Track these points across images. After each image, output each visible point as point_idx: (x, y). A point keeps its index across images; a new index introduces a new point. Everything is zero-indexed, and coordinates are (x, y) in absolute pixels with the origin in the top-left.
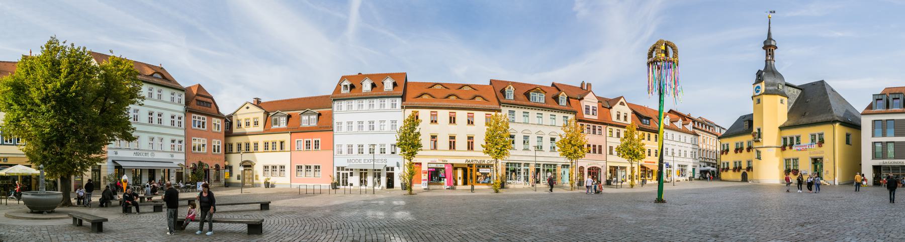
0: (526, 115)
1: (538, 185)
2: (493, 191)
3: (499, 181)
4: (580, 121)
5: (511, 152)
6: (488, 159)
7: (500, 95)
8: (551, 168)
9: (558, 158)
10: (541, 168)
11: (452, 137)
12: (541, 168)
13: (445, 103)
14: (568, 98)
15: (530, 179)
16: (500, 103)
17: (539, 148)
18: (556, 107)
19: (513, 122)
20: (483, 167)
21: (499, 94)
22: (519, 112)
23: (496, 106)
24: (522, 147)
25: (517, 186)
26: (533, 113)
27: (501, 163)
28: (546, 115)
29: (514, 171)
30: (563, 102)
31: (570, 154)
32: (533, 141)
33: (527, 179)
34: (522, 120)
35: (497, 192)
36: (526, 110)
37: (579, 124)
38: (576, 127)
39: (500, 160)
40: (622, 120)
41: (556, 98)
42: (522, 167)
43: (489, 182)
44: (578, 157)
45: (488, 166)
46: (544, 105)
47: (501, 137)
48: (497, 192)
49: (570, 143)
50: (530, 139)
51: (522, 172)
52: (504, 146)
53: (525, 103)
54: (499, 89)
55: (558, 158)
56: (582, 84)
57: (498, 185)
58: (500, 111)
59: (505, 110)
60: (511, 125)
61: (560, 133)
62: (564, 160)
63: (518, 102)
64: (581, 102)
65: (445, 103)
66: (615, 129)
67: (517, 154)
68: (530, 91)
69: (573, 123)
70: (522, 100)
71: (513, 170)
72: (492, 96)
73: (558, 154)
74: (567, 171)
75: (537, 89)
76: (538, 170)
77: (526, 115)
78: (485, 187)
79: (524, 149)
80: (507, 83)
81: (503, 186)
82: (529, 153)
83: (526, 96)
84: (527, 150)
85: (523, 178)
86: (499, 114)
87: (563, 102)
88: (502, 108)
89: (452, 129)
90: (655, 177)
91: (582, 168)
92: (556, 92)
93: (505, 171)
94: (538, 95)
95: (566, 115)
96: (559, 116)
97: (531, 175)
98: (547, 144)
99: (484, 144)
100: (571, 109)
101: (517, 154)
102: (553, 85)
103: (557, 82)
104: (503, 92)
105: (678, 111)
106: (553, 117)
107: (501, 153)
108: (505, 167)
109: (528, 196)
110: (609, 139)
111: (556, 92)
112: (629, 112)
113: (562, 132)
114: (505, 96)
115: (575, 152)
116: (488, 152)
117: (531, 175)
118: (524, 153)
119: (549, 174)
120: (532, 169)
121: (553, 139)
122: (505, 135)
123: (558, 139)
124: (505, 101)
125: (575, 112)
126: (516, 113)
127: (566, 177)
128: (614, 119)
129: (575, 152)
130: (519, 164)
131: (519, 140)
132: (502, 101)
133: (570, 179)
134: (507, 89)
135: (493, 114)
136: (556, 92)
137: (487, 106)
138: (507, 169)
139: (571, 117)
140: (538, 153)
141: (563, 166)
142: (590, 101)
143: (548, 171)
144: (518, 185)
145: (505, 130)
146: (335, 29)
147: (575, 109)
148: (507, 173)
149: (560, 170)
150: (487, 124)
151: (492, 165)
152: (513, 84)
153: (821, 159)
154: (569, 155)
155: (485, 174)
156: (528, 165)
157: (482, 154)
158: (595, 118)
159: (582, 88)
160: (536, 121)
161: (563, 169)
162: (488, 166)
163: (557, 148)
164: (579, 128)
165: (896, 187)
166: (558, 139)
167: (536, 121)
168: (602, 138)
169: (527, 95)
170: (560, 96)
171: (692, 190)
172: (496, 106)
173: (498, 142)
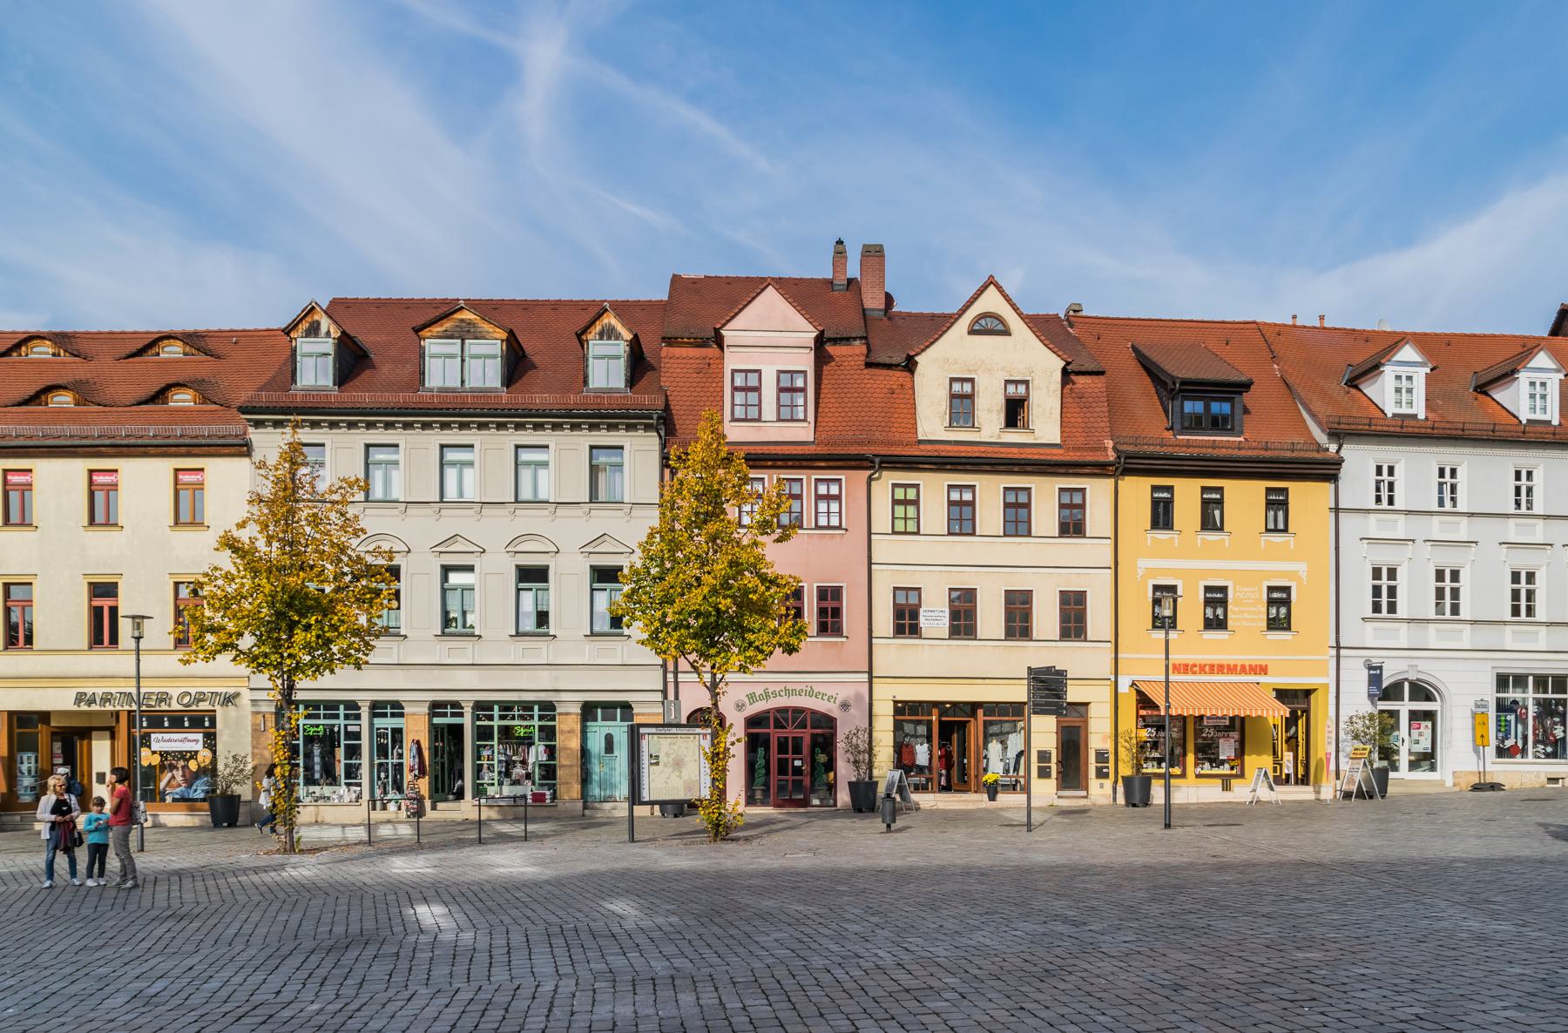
11: (103, 590)
13: (148, 427)
26: (417, 448)
28: (493, 448)
40: (989, 427)
61: (630, 532)
65: (148, 427)
66: (934, 489)
89: (103, 553)
90: (596, 777)
98: (569, 592)
105: (885, 372)
110: (884, 548)
112: (1042, 367)
120: (416, 728)
128: (932, 424)
142: (769, 342)
146: (468, 78)
158: (801, 432)
165: (996, 792)
168: (1091, 551)
171: (768, 874)
173: (302, 604)
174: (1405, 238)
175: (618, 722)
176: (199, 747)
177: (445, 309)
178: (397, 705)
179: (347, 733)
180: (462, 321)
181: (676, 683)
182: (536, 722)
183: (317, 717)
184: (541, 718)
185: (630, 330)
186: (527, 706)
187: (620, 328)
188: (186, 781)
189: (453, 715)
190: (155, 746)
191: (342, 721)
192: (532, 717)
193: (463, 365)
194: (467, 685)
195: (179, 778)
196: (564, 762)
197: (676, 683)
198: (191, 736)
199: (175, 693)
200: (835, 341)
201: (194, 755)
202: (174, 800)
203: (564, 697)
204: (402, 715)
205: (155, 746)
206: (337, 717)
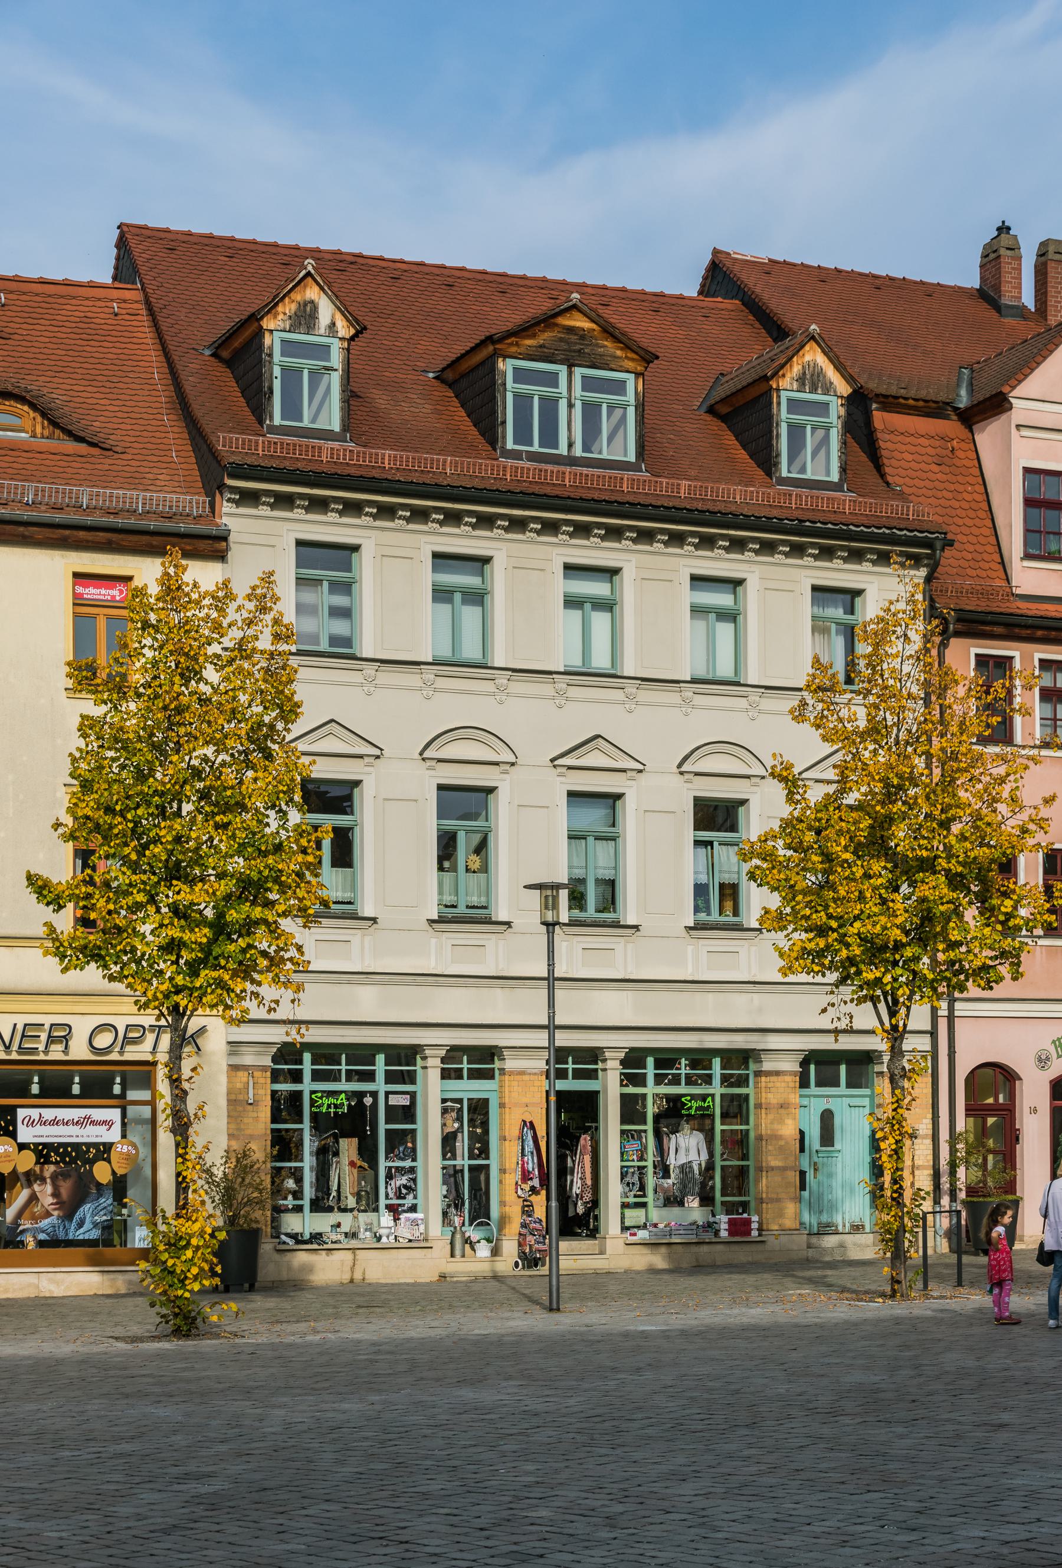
0: (461, 581)
1: (574, 1256)
2: (145, 1318)
3: (209, 1217)
4: (973, 624)
5: (317, 945)
6: (97, 1013)
7: (213, 387)
8: (698, 1086)
9: (760, 992)
10: (611, 1086)
12: (611, 1086)
14: (859, 402)
15: (506, 1193)
16: (214, 473)
17: (589, 901)
18: (743, 494)
19: (342, 651)
20: (56, 1087)
21: (199, 370)
22: (394, 562)
23: (175, 497)
24: (426, 889)
25: (379, 1268)
26: (527, 569)
27: (223, 1056)
28: (656, 579)
29: (355, 1121)
30: (815, 456)
31: (877, 950)
32: (531, 840)
33: (469, 1196)
34: (423, 630)
35: (185, 1322)
36: (462, 540)
37: (964, 656)
38: (935, 690)
39: (214, 1030)
41: (745, 414)
42: (432, 1087)
43: (114, 1232)
44: (954, 979)
45: (99, 1082)
46: (635, 485)
47: (223, 805)
48: (185, 1322)
49: (876, 843)
50: (504, 818)
51: (430, 1126)
52: (251, 889)
53: (448, 467)
54: (200, 331)
55: (760, 992)
56: (998, 253)
57: (195, 1266)
58: (212, 546)
59: (264, 542)
60: (318, 692)
61: (782, 752)
62: (811, 1011)
63: (387, 459)
64: (987, 437)
67: (375, 963)
68: (495, 344)
69: (904, 656)
70: (427, 435)
71: (339, 1114)
72: (135, 405)
73: (759, 956)
74: (855, 1114)
75: (562, 322)
76: (576, 1114)
77: (461, 581)
78: (79, 1281)
79: (449, 918)
80: (280, 266)
81: (241, 1262)
82: (492, 953)
83: (456, 402)
84: (480, 918)
85: (433, 1190)
86: (202, 575)
87: (815, 456)
88: (232, 518)
91: (993, 1084)
92: (741, 353)
93: (261, 1120)
94: (570, 385)
95: (839, 574)
96: (780, 591)
97: (508, 1161)
98: (658, 863)
99: (61, 867)
100: (889, 509)
101: (375, 963)
102: (720, 275)
103: (753, 246)
104: (240, 352)
106: (720, 604)
107: (221, 953)
108: (262, 1092)
109: (483, 1359)
111: (748, 351)
113: (807, 748)
114: (257, 399)
115: (926, 928)
116: (97, 942)
117: (508, 1161)
118: (443, 951)
119: (688, 1148)
120: (522, 1099)
121: (716, 816)
122: (256, 784)
123: (765, 812)
124: (259, 448)
125: (921, 547)
126: (367, 568)
127: (850, 1160)
129: (926, 928)
130: (404, 1059)
131: (395, 827)
132: (229, 443)
133: (884, 1186)
134: (276, 331)
135: (147, 572)
136: (741, 353)
137: (88, 497)
138: (286, 1107)
139: (886, 590)
140: (575, 954)
141: (822, 1067)
143: (673, 1114)
144: (392, 1253)
145: (261, 741)
147: (923, 510)
148: (284, 1146)
149: (785, 1110)
150: (84, 675)
151: (141, 1074)
152: (342, 271)
153: (716, 252)
154: (864, 963)
155: (71, 1162)
156: (483, 1060)
157: (40, 969)
159: (989, 296)
160: (560, 640)
161: (819, 1099)
162: (99, 1082)
163: (758, 899)
164: (962, 701)
166: (765, 812)
167: (560, 640)
169: (470, 383)
170: (787, 386)
172: (175, 497)
174: (704, 111)
175: (842, 1089)
176: (113, 1135)
177: (543, 305)
178: (490, 1053)
179: (389, 1108)
180: (571, 330)
181: (951, 1018)
182: (717, 1089)
183: (335, 1077)
184: (725, 1080)
185: (849, 378)
186: (700, 1059)
187: (831, 373)
188: (60, 1204)
189: (579, 1075)
190: (25, 1134)
191: (380, 1085)
192: (708, 1080)
193: (583, 417)
194: (610, 1015)
195: (47, 1199)
196: (774, 1163)
197: (951, 1018)
198: (98, 1114)
199: (81, 1028)
200: (891, 403)
201: (104, 1150)
202: (41, 1244)
203: (774, 1042)
204: (488, 1075)
205: (25, 1134)
206: (370, 1076)
